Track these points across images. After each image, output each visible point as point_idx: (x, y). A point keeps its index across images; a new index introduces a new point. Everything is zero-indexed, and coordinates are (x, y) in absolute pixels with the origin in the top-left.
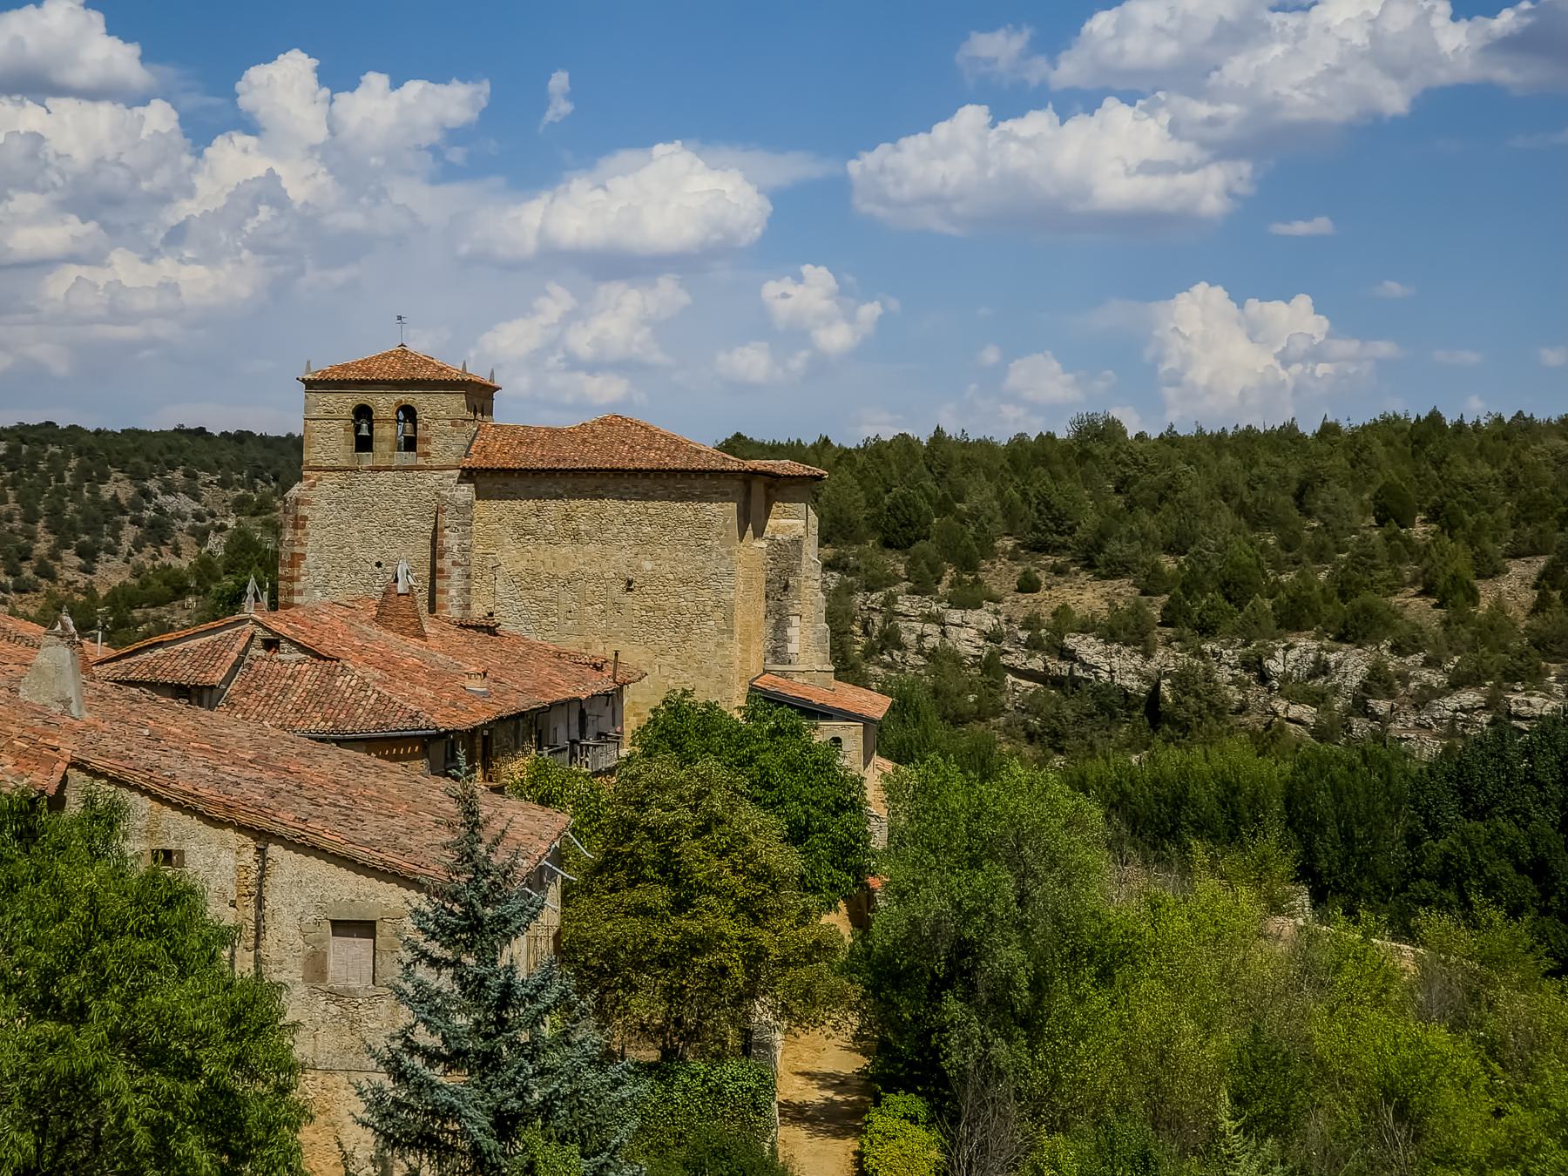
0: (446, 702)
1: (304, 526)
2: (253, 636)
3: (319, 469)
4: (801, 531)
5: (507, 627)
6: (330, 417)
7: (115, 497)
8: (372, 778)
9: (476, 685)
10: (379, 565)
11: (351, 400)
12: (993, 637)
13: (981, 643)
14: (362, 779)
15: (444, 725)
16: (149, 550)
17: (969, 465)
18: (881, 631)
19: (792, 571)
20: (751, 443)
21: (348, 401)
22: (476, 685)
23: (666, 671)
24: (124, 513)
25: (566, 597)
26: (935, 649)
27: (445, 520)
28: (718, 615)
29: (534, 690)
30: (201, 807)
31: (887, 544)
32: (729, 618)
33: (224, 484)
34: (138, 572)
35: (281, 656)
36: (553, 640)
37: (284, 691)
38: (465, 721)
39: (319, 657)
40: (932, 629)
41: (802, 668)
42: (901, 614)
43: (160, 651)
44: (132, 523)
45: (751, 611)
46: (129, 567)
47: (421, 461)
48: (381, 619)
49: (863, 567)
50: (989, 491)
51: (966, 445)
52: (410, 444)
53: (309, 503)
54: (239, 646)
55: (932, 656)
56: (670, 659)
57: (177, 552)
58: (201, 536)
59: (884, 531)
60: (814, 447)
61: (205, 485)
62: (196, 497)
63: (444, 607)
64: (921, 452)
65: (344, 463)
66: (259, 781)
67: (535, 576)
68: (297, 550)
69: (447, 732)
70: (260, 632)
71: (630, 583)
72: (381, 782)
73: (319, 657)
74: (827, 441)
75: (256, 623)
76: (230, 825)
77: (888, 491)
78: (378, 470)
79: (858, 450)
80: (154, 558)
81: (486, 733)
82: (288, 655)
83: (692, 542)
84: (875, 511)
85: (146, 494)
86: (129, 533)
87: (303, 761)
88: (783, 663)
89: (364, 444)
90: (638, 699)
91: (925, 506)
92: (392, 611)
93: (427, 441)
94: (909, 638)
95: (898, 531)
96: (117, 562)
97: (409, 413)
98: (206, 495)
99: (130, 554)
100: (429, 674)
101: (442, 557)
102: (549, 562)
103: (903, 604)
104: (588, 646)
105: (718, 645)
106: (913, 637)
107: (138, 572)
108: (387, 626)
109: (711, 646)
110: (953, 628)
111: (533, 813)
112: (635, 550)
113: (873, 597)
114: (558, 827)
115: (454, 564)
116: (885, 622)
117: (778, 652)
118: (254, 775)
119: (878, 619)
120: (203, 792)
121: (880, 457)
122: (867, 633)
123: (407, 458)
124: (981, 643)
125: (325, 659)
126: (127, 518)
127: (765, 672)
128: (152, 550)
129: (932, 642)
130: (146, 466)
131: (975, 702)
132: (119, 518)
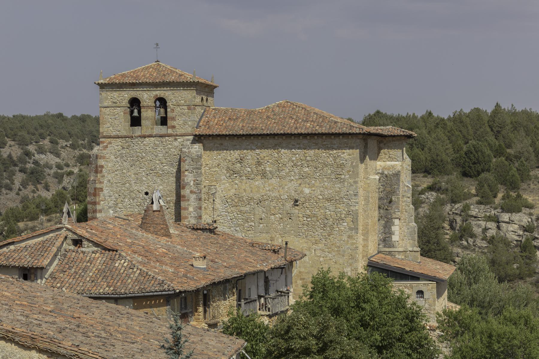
0: (181, 274)
1: (101, 171)
2: (66, 238)
3: (110, 137)
4: (399, 168)
5: (220, 228)
6: (115, 105)
7: (10, 156)
8: (125, 320)
9: (201, 264)
10: (147, 194)
11: (127, 95)
12: (527, 229)
13: (521, 233)
14: (119, 321)
15: (178, 288)
16: (31, 187)
17: (516, 126)
18: (460, 227)
19: (393, 192)
20: (385, 116)
21: (127, 95)
22: (201, 264)
23: (318, 253)
24: (15, 165)
25: (260, 211)
26: (493, 237)
27: (185, 166)
28: (349, 219)
29: (236, 266)
30: (17, 339)
31: (465, 174)
32: (355, 221)
33: (73, 147)
34: (24, 200)
35: (83, 249)
36: (251, 236)
37: (85, 270)
38: (191, 286)
39: (105, 249)
40: (492, 225)
41: (401, 249)
42: (472, 216)
43: (12, 247)
44: (20, 171)
45: (369, 214)
46: (20, 198)
47: (170, 131)
48: (143, 226)
49: (450, 189)
50: (527, 141)
51: (514, 114)
52: (164, 121)
53: (104, 157)
54: (58, 244)
55: (491, 241)
56: (321, 246)
57: (47, 188)
58: (59, 178)
59: (463, 167)
60: (422, 117)
61: (62, 147)
62: (58, 155)
63: (186, 218)
64: (486, 119)
65: (125, 133)
66: (54, 323)
67: (240, 199)
68: (98, 186)
69: (180, 292)
70: (70, 235)
71: (296, 201)
72: (130, 322)
73: (105, 249)
74: (430, 114)
75: (68, 229)
76: (34, 348)
77: (466, 143)
78: (144, 137)
79: (449, 119)
80: (34, 192)
81: (205, 292)
82: (87, 248)
83: (333, 176)
84: (458, 155)
85: (28, 154)
86: (19, 178)
87: (83, 311)
88: (390, 247)
89: (136, 122)
90: (303, 270)
91: (488, 152)
92: (149, 220)
93: (173, 119)
94: (477, 231)
95: (471, 166)
96: (12, 194)
97: (162, 102)
98: (64, 154)
99: (20, 190)
100: (172, 258)
101: (184, 188)
102: (248, 189)
103: (474, 211)
104: (272, 239)
105: (349, 237)
106: (480, 230)
107: (24, 200)
108: (147, 230)
109: (345, 238)
110: (504, 225)
111: (222, 339)
112: (299, 182)
113: (456, 206)
114: (235, 347)
115: (191, 192)
116: (463, 221)
117: (386, 240)
118: (51, 320)
119: (459, 219)
120: (18, 330)
121: (461, 122)
122: (452, 228)
123: (162, 130)
124: (521, 233)
125: (109, 250)
126: (17, 168)
127: (379, 252)
128: (32, 187)
129: (492, 232)
130: (27, 137)
131: (518, 268)
132: (12, 168)
